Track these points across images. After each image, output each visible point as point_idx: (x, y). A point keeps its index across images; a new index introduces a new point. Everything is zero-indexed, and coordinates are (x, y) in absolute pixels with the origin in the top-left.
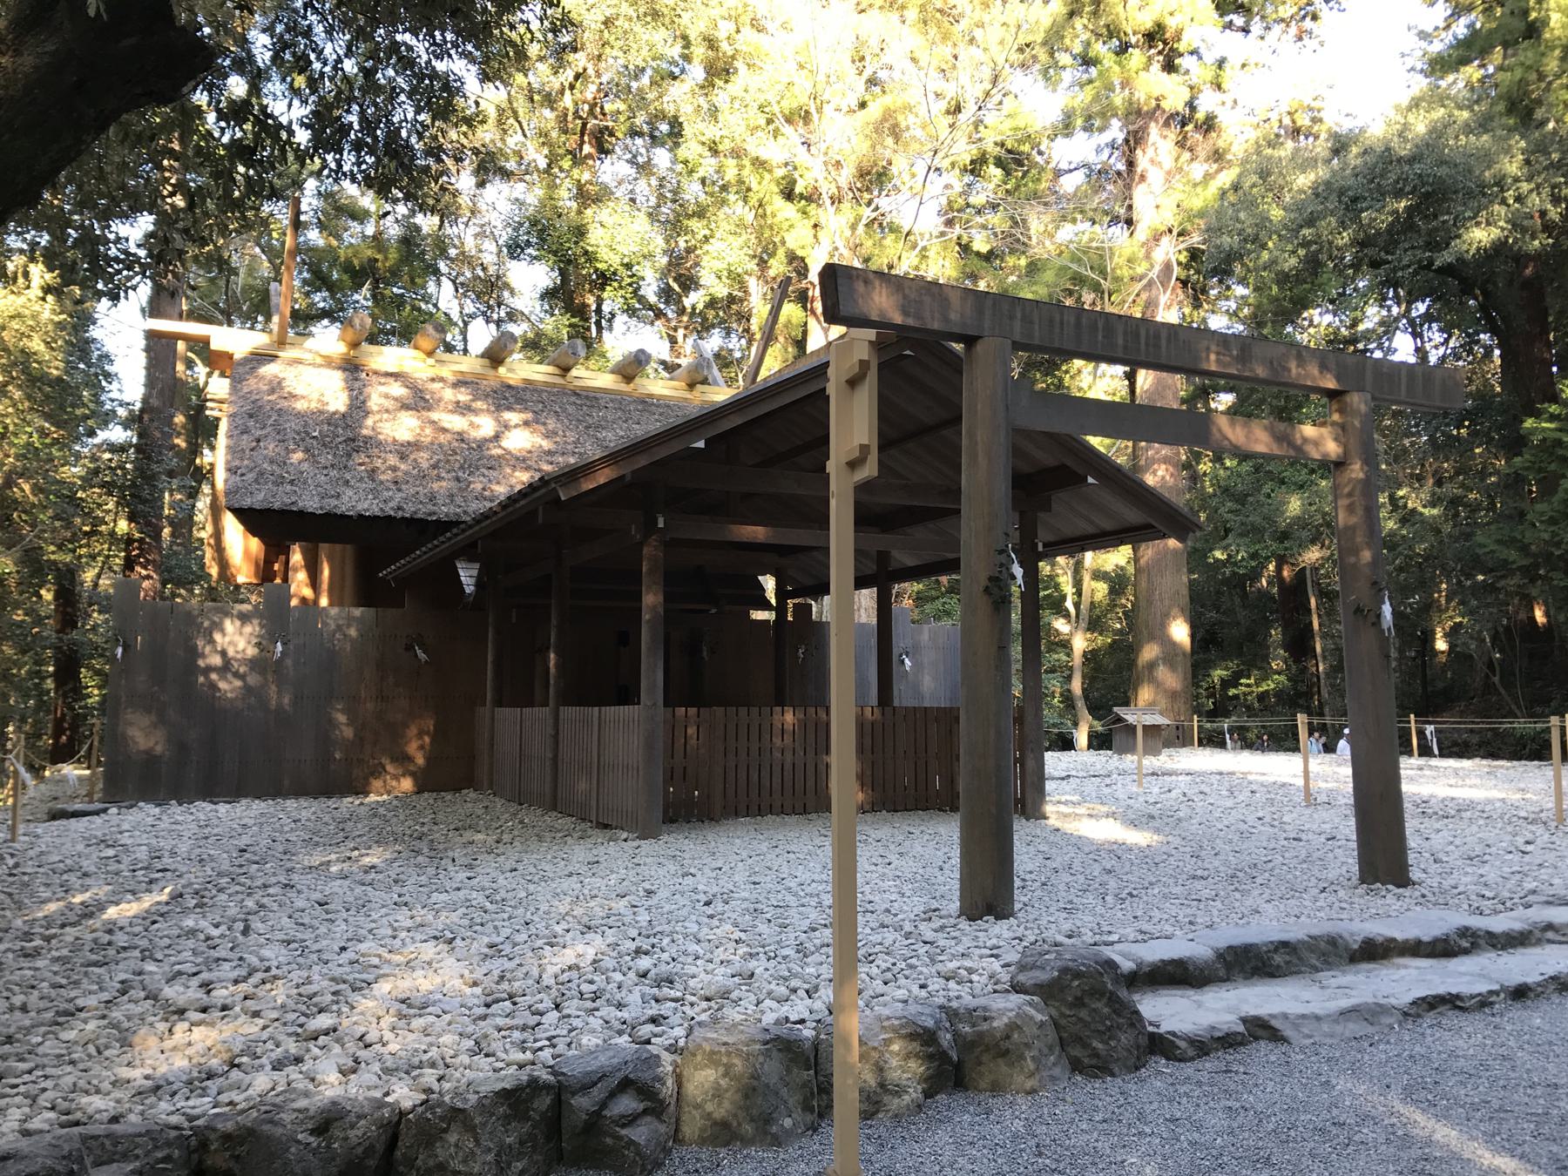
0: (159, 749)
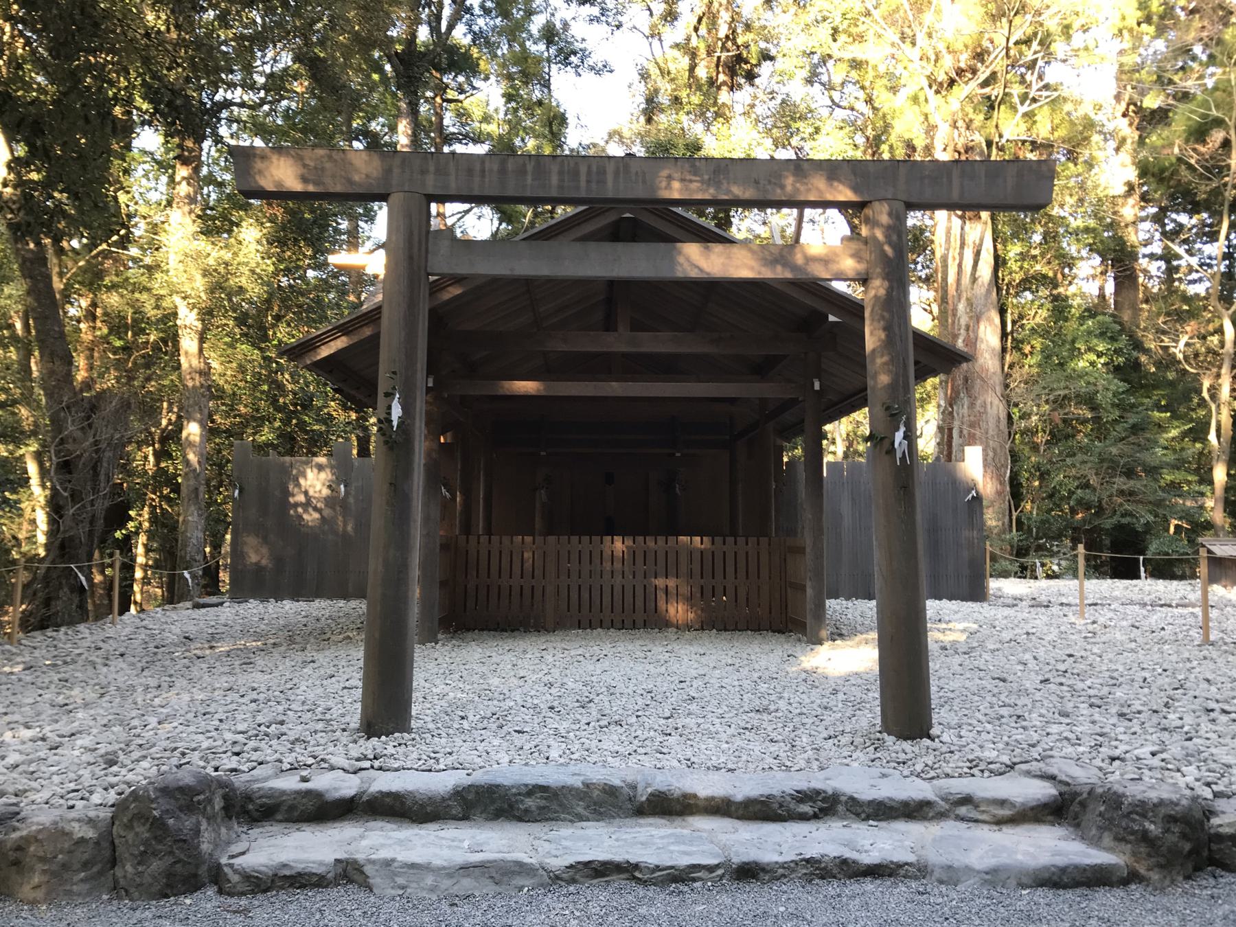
0: (264, 562)
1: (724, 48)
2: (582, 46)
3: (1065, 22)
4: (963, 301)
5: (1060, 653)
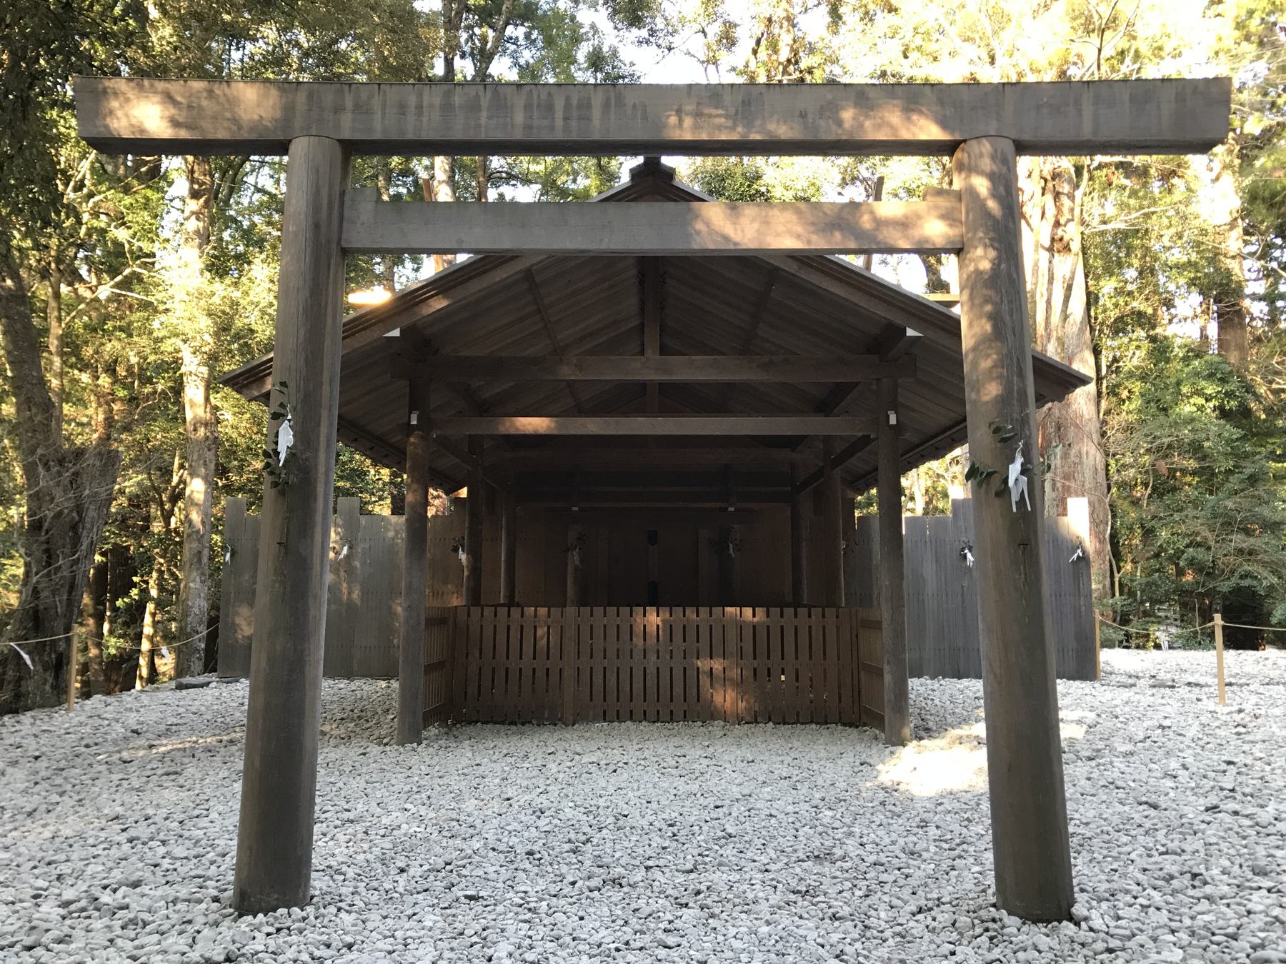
1: (785, 72)
2: (630, 70)
3: (1155, 45)
4: (1053, 340)
5: (1216, 759)
